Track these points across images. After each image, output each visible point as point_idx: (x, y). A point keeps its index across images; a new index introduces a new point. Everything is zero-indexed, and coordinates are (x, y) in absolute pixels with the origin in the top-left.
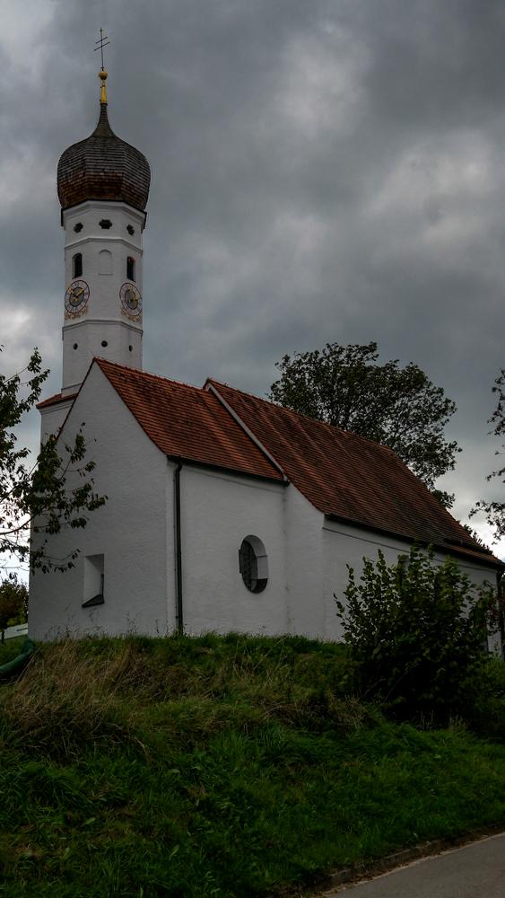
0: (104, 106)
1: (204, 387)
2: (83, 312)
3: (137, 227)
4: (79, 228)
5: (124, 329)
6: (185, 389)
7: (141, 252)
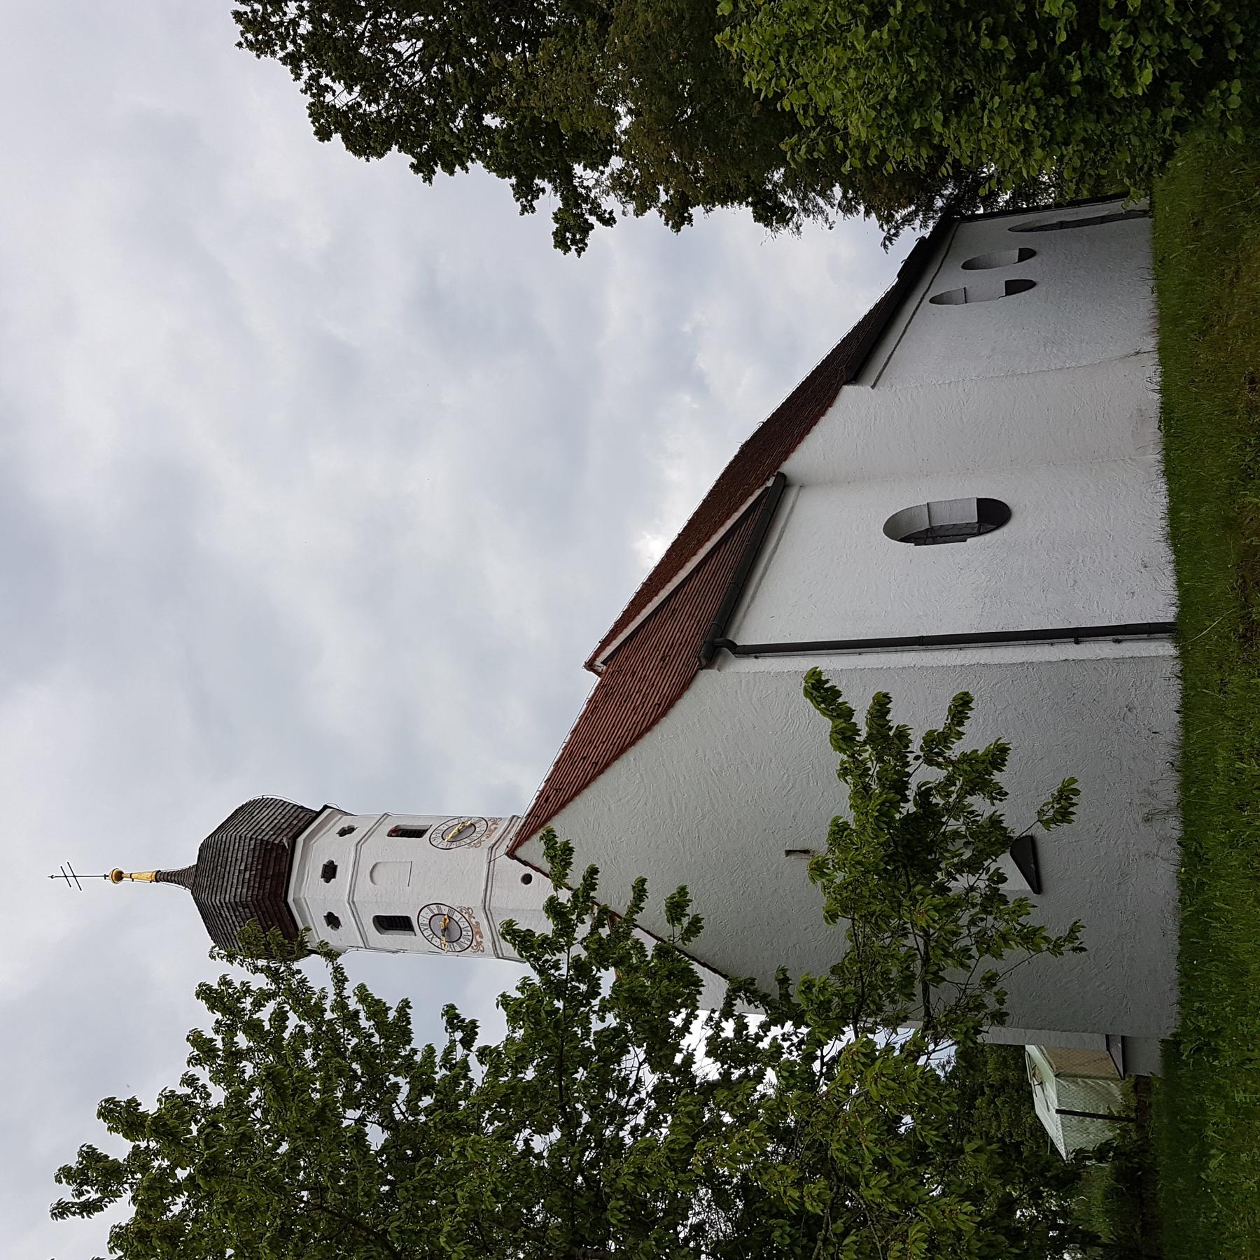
0: (160, 877)
1: (599, 674)
2: (470, 916)
3: (345, 822)
4: (333, 921)
5: (949, 278)
6: (594, 705)
7: (386, 815)
